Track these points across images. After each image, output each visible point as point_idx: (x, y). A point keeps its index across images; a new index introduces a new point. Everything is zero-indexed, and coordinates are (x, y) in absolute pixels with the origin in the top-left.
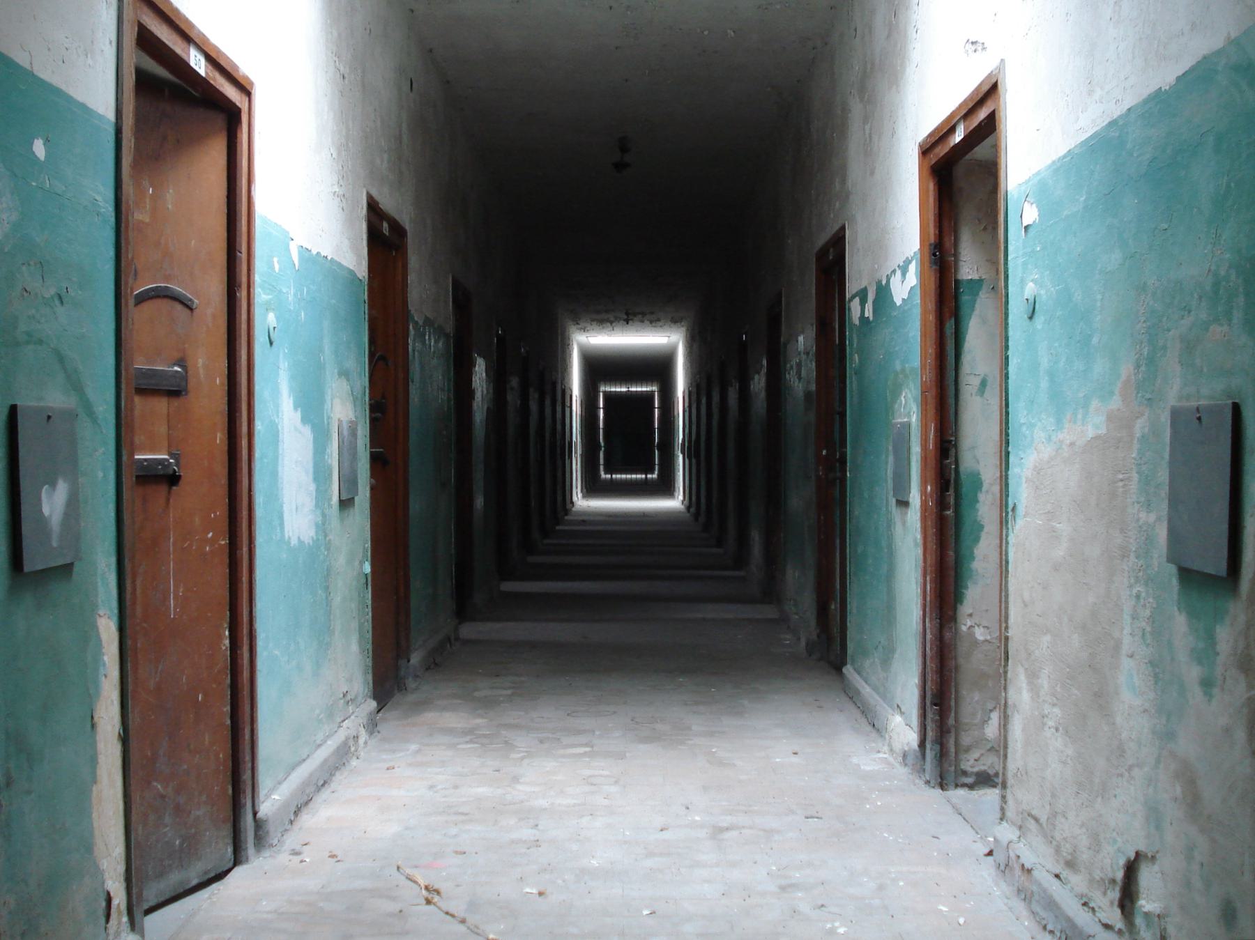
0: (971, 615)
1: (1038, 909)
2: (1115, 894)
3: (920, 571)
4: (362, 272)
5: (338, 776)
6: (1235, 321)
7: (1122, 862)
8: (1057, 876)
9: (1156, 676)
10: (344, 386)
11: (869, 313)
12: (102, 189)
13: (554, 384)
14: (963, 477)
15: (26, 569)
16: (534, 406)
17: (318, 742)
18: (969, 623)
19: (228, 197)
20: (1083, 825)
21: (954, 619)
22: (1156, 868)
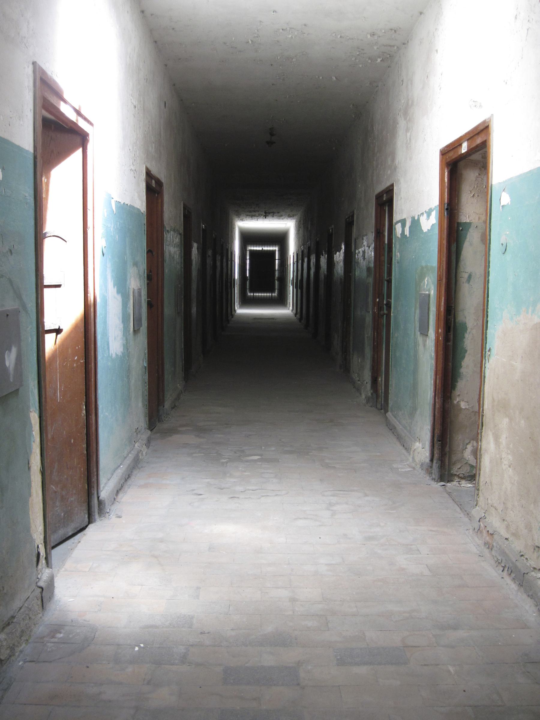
0: (459, 395)
3: (433, 374)
11: (407, 232)
13: (227, 250)
16: (218, 264)
17: (125, 456)
18: (458, 400)
21: (450, 397)
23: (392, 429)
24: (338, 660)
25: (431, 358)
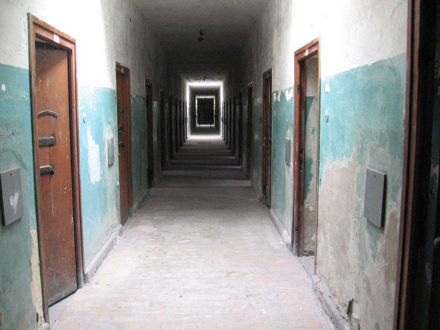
0: (308, 203)
1: (324, 306)
2: (346, 309)
4: (114, 88)
5: (111, 253)
6: (386, 148)
7: (348, 300)
8: (330, 297)
9: (360, 248)
10: (110, 127)
11: (279, 100)
12: (26, 93)
13: (180, 101)
14: (306, 159)
15: (6, 225)
16: (173, 111)
19: (69, 78)
21: (303, 204)
23: (273, 220)
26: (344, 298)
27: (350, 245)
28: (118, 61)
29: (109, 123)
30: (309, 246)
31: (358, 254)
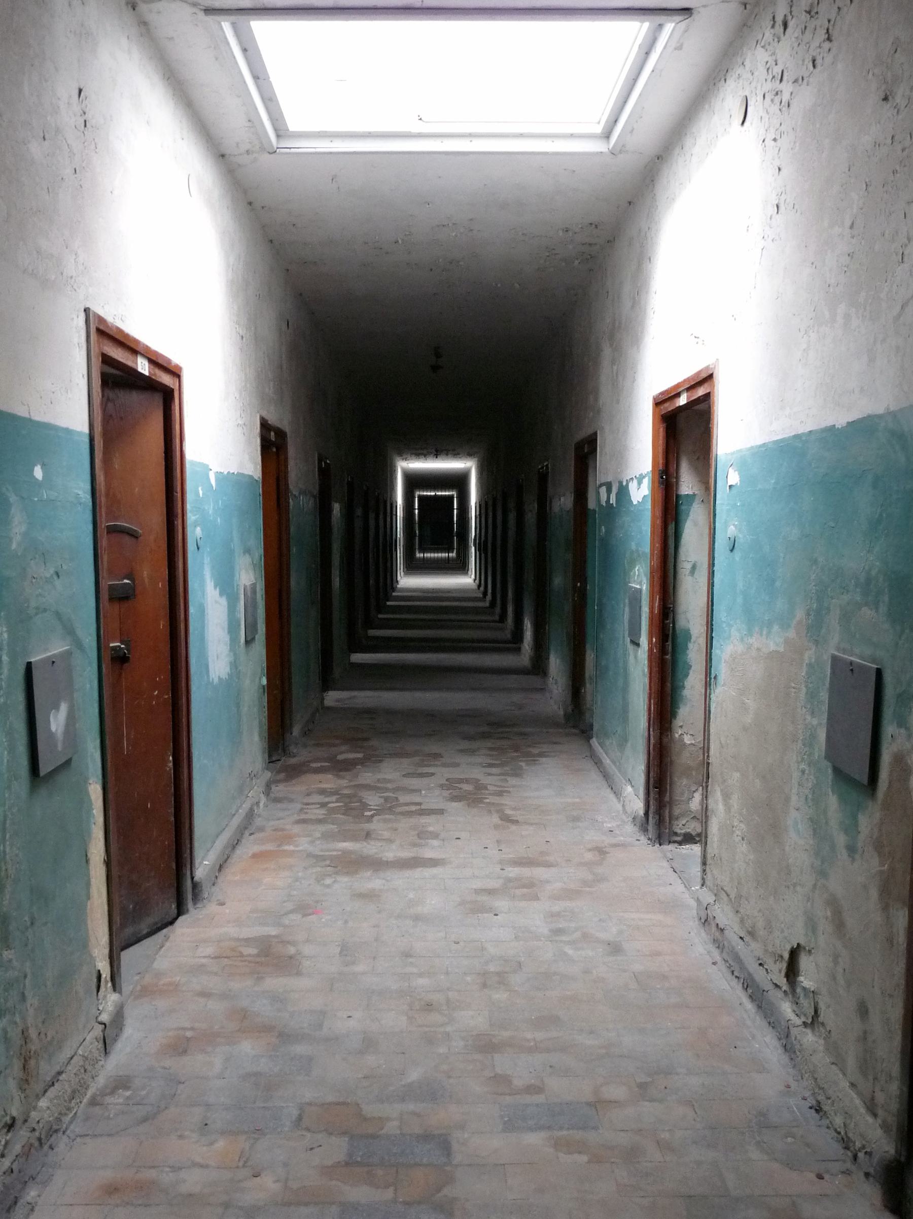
0: (681, 727)
3: (646, 696)
6: (881, 610)
7: (788, 948)
9: (814, 830)
11: (613, 500)
12: (82, 485)
13: (385, 502)
15: (42, 774)
16: (372, 523)
20: (760, 911)
22: (811, 958)
24: (505, 1123)
25: (644, 674)
26: (777, 942)
27: (790, 822)
28: (265, 414)
29: (247, 551)
30: (684, 822)
31: (811, 842)
